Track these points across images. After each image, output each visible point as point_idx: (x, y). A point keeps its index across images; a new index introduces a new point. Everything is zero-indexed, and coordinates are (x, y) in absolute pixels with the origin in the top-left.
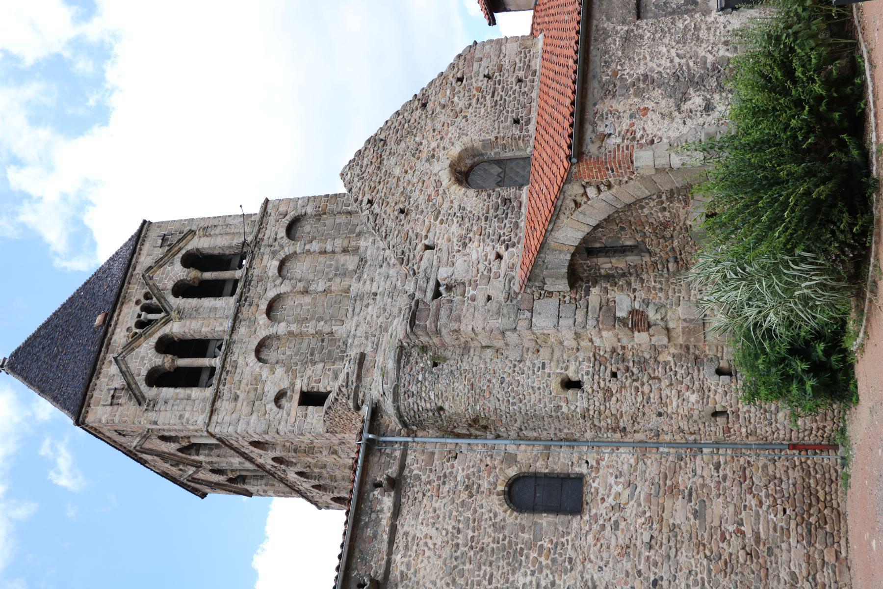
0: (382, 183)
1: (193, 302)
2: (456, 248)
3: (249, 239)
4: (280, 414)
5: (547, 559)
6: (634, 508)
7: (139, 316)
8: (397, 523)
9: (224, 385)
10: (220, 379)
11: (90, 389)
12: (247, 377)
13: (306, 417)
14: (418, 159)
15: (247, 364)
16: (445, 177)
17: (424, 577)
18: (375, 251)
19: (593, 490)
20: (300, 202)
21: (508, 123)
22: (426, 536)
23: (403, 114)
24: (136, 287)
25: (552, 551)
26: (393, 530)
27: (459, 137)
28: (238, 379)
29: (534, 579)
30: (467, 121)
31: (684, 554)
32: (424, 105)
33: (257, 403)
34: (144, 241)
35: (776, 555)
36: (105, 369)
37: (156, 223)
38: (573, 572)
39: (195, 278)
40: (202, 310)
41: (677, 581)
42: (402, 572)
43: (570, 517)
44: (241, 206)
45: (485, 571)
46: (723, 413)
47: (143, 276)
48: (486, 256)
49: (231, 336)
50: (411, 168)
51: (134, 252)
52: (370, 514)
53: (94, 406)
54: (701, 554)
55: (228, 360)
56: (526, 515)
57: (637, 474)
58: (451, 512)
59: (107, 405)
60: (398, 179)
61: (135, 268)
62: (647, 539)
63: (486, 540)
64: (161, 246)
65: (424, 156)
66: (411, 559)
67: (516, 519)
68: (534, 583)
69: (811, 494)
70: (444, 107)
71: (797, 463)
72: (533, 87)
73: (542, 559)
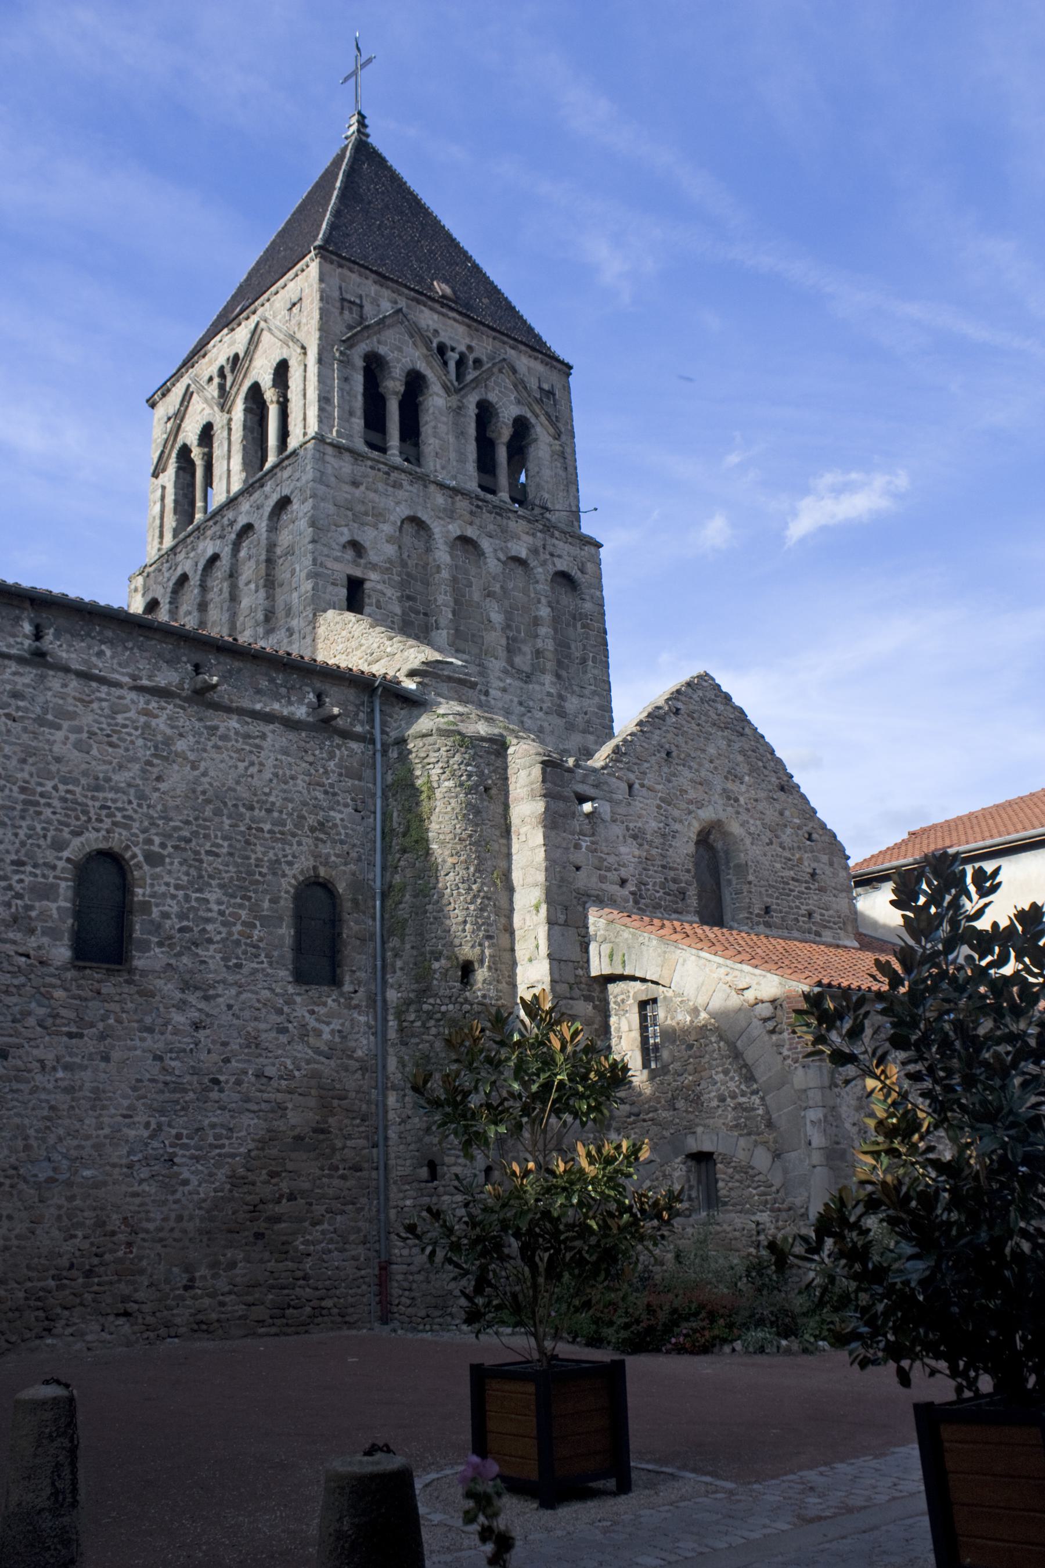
0: (697, 728)
1: (472, 430)
2: (631, 825)
6: (304, 1055)
7: (453, 349)
10: (378, 462)
12: (384, 502)
13: (333, 584)
14: (726, 778)
15: (398, 503)
16: (707, 814)
19: (324, 999)
20: (598, 593)
21: (765, 899)
22: (261, 764)
23: (772, 760)
24: (490, 348)
25: (249, 941)
26: (269, 718)
27: (750, 834)
29: (214, 915)
30: (768, 844)
31: (252, 1122)
32: (782, 789)
34: (547, 364)
35: (255, 1244)
36: (386, 293)
38: (224, 969)
39: (500, 433)
40: (463, 441)
41: (219, 1112)
42: (216, 728)
43: (290, 967)
44: (596, 509)
45: (222, 846)
46: (433, 1176)
47: (504, 360)
48: (624, 866)
49: (434, 482)
52: (285, 687)
53: (340, 274)
54: (251, 1146)
55: (403, 476)
56: (291, 906)
57: (345, 1060)
58: (291, 801)
59: (341, 294)
63: (259, 848)
64: (540, 388)
65: (730, 785)
66: (233, 742)
67: (287, 892)
68: (210, 915)
69: (328, 1290)
71: (363, 1272)
72: (804, 932)
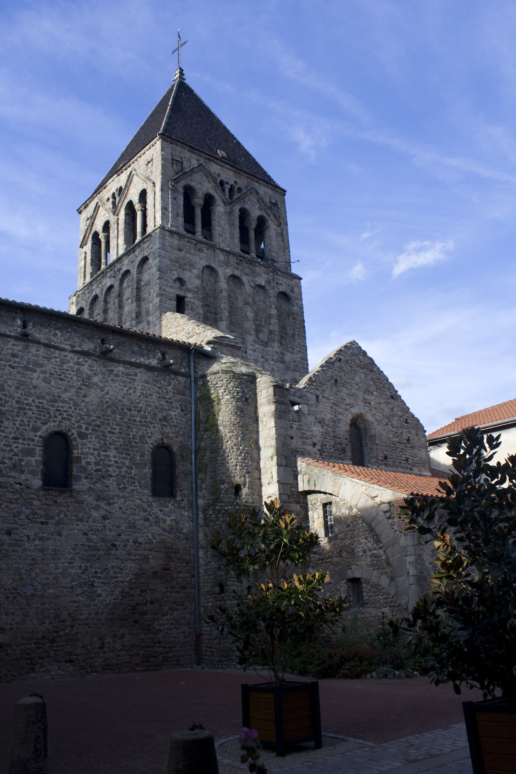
0: (350, 368)
1: (237, 223)
2: (318, 417)
4: (171, 281)
5: (125, 472)
7: (227, 183)
8: (142, 369)
11: (182, 145)
13: (170, 299)
16: (355, 410)
17: (111, 386)
18: (272, 354)
19: (167, 504)
20: (300, 302)
21: (385, 452)
22: (135, 388)
24: (245, 182)
25: (129, 476)
26: (138, 365)
28: (192, 252)
29: (113, 463)
30: (386, 425)
31: (132, 565)
32: (392, 398)
33: (177, 264)
34: (273, 190)
36: (194, 156)
37: (284, 199)
38: (118, 490)
39: (251, 224)
40: (233, 228)
41: (116, 560)
42: (113, 371)
43: (150, 488)
44: (299, 261)
46: (222, 591)
47: (253, 188)
48: (315, 436)
49: (218, 249)
50: (359, 388)
51: (267, 183)
52: (146, 350)
53: (171, 147)
55: (203, 246)
57: (178, 534)
58: (150, 406)
59: (172, 157)
60: (353, 379)
61: (257, 182)
62: (140, 540)
63: (134, 430)
64: (271, 202)
65: (366, 396)
66: (121, 378)
68: (110, 463)
70: (392, 410)
71: (188, 639)
73: (125, 469)
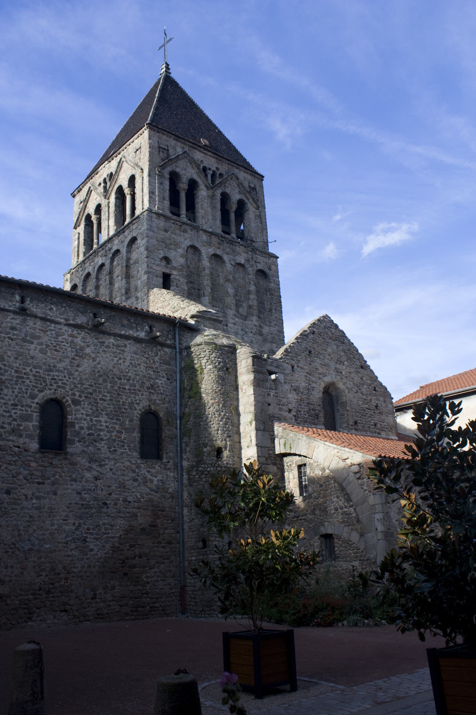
0: (323, 340)
1: (219, 206)
2: (293, 385)
3: (256, 245)
4: (158, 260)
5: (115, 436)
7: (210, 169)
8: (131, 341)
9: (173, 223)
11: (168, 134)
13: (156, 276)
14: (336, 363)
15: (185, 239)
16: (328, 379)
17: (102, 357)
18: (251, 327)
20: (277, 279)
21: (355, 418)
22: (125, 359)
24: (226, 168)
25: (119, 439)
26: (127, 338)
27: (347, 388)
28: (177, 233)
29: (104, 428)
30: (356, 393)
31: (122, 522)
32: (362, 367)
33: (163, 244)
34: (252, 176)
36: (179, 144)
37: (262, 184)
38: (109, 452)
39: (231, 207)
40: (215, 211)
41: (107, 518)
42: (104, 342)
43: (139, 451)
44: (275, 241)
46: (205, 546)
48: (290, 403)
49: (201, 230)
50: (332, 358)
51: (246, 169)
52: (135, 323)
53: (158, 136)
55: (188, 227)
57: (164, 493)
58: (138, 375)
59: (159, 145)
60: (326, 350)
61: (237, 169)
62: (130, 499)
63: (124, 397)
64: (250, 187)
65: (338, 366)
66: (112, 349)
68: (102, 427)
70: (362, 379)
71: (173, 590)
73: (115, 433)
